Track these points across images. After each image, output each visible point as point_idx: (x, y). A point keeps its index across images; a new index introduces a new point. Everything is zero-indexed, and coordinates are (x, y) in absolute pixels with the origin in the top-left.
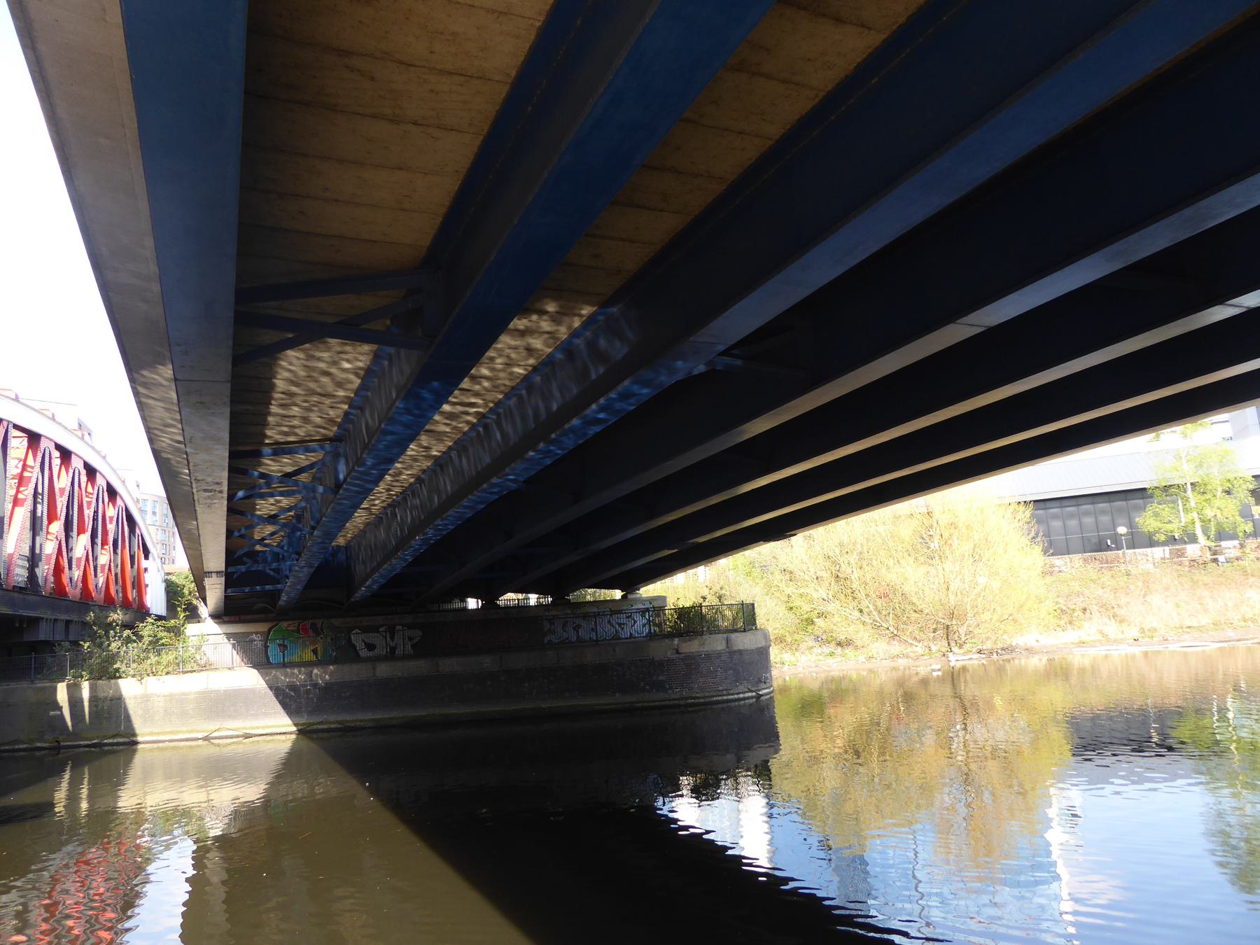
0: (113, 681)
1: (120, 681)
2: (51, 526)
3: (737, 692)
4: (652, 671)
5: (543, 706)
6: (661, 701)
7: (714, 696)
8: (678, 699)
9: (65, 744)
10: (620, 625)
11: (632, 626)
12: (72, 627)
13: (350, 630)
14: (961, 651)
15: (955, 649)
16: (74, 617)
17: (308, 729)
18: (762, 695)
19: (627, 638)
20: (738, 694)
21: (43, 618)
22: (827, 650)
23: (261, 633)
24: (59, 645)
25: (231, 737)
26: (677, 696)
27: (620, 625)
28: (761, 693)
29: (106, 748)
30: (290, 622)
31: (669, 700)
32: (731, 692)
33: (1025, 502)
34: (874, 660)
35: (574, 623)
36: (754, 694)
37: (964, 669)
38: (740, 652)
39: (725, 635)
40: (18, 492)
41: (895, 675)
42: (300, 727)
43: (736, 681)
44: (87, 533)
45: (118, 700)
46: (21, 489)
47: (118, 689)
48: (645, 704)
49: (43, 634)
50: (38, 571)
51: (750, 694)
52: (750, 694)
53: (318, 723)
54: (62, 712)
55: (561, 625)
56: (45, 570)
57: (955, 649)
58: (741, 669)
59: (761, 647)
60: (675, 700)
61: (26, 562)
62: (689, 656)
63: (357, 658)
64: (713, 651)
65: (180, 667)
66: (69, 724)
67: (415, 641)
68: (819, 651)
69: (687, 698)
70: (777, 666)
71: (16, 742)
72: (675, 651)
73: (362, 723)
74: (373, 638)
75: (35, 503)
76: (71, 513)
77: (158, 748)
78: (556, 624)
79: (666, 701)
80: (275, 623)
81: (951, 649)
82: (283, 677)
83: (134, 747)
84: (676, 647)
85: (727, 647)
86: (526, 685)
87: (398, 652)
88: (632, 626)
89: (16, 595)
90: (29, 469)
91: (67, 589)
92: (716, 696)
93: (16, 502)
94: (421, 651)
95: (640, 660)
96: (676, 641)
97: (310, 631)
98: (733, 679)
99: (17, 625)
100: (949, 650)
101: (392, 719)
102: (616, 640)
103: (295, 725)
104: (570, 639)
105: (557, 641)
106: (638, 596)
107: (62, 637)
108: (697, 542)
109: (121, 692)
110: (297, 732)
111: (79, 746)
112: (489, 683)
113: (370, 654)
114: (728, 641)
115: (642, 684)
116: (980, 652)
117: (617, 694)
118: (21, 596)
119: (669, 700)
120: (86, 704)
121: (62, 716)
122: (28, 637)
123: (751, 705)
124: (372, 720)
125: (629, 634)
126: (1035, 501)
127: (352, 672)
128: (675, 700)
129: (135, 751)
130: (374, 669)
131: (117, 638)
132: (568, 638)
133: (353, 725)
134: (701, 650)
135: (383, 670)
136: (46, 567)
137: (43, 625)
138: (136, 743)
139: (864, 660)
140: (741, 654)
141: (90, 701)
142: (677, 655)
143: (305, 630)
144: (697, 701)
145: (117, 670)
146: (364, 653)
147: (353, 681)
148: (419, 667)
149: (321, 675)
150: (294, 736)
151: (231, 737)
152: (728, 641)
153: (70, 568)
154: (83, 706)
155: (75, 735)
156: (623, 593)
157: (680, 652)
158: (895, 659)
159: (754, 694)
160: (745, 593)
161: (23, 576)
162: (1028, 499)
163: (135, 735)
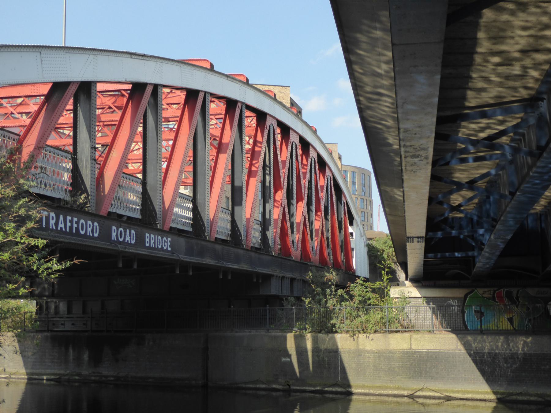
0: (330, 335)
12: (295, 284)
16: (297, 276)
17: (508, 398)
30: (486, 290)
42: (499, 396)
45: (335, 353)
46: (254, 162)
47: (335, 343)
49: (274, 289)
54: (291, 358)
66: (297, 370)
76: (291, 183)
80: (470, 290)
89: (253, 254)
103: (495, 393)
109: (337, 346)
111: (305, 391)
118: (257, 255)
120: (310, 354)
122: (263, 292)
129: (350, 400)
131: (332, 296)
137: (274, 281)
138: (351, 394)
141: (313, 351)
145: (334, 326)
150: (494, 404)
154: (307, 356)
155: (301, 381)
161: (256, 238)
163: (349, 386)
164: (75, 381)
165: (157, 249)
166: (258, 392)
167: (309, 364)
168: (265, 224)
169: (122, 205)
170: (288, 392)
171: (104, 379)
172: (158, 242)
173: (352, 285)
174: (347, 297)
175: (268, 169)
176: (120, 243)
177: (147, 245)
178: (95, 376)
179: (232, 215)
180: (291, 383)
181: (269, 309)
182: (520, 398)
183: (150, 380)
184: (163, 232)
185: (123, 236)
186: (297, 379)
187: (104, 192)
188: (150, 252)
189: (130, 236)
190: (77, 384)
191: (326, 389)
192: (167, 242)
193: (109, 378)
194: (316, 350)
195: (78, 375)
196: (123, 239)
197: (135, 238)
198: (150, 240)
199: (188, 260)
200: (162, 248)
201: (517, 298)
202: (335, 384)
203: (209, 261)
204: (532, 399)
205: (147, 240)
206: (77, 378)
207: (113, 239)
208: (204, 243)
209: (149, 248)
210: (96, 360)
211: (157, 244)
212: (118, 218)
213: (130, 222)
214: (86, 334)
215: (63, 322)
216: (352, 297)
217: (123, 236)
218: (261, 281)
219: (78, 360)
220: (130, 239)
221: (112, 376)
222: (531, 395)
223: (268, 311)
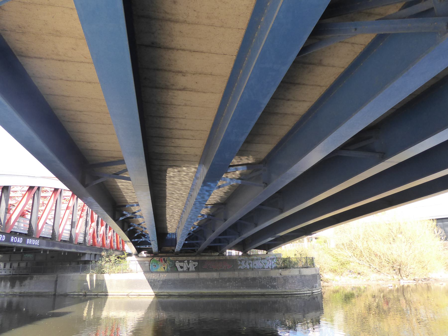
0: (102, 274)
1: (104, 274)
2: (92, 224)
3: (304, 291)
4: (272, 281)
5: (233, 291)
6: (275, 292)
7: (294, 292)
8: (281, 292)
9: (88, 294)
10: (265, 263)
11: (269, 264)
12: (97, 256)
13: (175, 261)
14: (407, 279)
15: (404, 278)
16: (98, 253)
17: (158, 294)
18: (314, 293)
19: (267, 268)
20: (304, 291)
21: (87, 253)
22: (354, 276)
23: (148, 261)
24: (91, 262)
25: (135, 295)
26: (281, 291)
27: (265, 263)
28: (314, 292)
29: (99, 296)
30: (157, 258)
31: (278, 292)
32: (301, 290)
33: (433, 219)
34: (369, 281)
35: (248, 262)
36: (311, 292)
37: (408, 286)
38: (305, 276)
39: (299, 269)
40: (81, 213)
41: (379, 287)
42: (156, 294)
43: (303, 287)
44: (104, 226)
45: (103, 281)
46: (82, 213)
47: (104, 277)
48: (269, 293)
49: (87, 258)
50: (87, 238)
51: (309, 292)
52: (309, 292)
53: (161, 293)
54: (87, 283)
55: (244, 263)
56: (89, 238)
57: (404, 278)
58: (305, 282)
59: (314, 274)
60: (280, 292)
61: (83, 235)
62: (285, 276)
63: (177, 271)
64: (293, 275)
65: (123, 271)
66: (89, 287)
67: (196, 266)
68: (351, 276)
69: (284, 292)
70: (331, 281)
71: (74, 292)
72: (280, 274)
73: (174, 294)
74: (181, 264)
75: (87, 217)
76: (99, 220)
77: (114, 297)
78: (242, 262)
79: (276, 292)
80: (152, 258)
81: (402, 278)
82: (154, 276)
83: (107, 296)
84: (280, 273)
85: (300, 273)
86: (228, 283)
87: (190, 270)
88: (269, 264)
89: (78, 246)
90: (85, 207)
91: (96, 244)
92: (295, 292)
93: (81, 217)
94: (198, 269)
95: (267, 277)
96: (280, 270)
97: (163, 261)
98: (302, 286)
99: (78, 255)
100: (402, 279)
101: (183, 293)
102: (263, 269)
103: (154, 293)
104: (247, 268)
105: (243, 268)
106: (272, 253)
107: (93, 259)
108: (280, 235)
109: (104, 278)
110: (155, 295)
111: (92, 295)
112: (215, 282)
113: (182, 270)
114: (299, 271)
115: (268, 286)
116: (414, 280)
117: (242, 287)
118: (80, 246)
119: (278, 292)
120: (94, 281)
121: (87, 284)
122: (82, 259)
123: (309, 296)
124: (178, 293)
125: (268, 267)
126: (437, 219)
127: (173, 276)
128: (280, 292)
129: (107, 298)
130: (179, 275)
131: (104, 261)
132: (246, 267)
133: (171, 294)
134: (289, 274)
135: (182, 276)
136: (89, 237)
137: (87, 255)
138: (107, 295)
139: (365, 281)
140: (305, 277)
141: (96, 281)
142: (281, 276)
143: (162, 261)
144: (288, 293)
145: (103, 271)
146: (180, 269)
147: (172, 279)
148: (193, 275)
149: (164, 276)
150: (154, 297)
151: (135, 295)
152: (299, 271)
153: (97, 237)
154: (93, 282)
155: (91, 291)
156: (242, 253)
157: (281, 274)
158: (378, 281)
159: (311, 292)
160: (311, 254)
161: (81, 240)
162: (434, 218)
163: (107, 292)
164: (3, 295)
165: (32, 245)
166: (74, 296)
167: (94, 285)
168: (85, 234)
169: (19, 229)
170: (85, 295)
171: (15, 293)
172: (33, 242)
173: (111, 257)
174: (109, 261)
175: (88, 215)
176: (15, 243)
177: (28, 243)
178: (11, 292)
179: (71, 231)
180: (86, 292)
181: (82, 266)
182: (162, 294)
183: (34, 293)
184: (35, 239)
185: (16, 240)
186: (89, 291)
187: (10, 224)
188: (29, 246)
189: (20, 240)
190: (3, 296)
191: (99, 294)
192: (37, 242)
193: (17, 293)
194: (97, 280)
195: (4, 292)
196: (16, 241)
197: (22, 241)
198: (29, 241)
199: (46, 248)
200: (35, 244)
201: (167, 260)
202: (75, 292)
203: (57, 248)
204: (165, 294)
205: (28, 241)
206: (4, 293)
207: (11, 241)
208: (55, 242)
209: (29, 244)
210: (13, 286)
211: (33, 243)
212: (15, 234)
213: (21, 234)
214: (10, 276)
215: (1, 271)
216: (111, 261)
217: (16, 240)
218: (81, 255)
219: (5, 286)
220: (20, 241)
221: (19, 292)
222: (165, 293)
223: (81, 266)
